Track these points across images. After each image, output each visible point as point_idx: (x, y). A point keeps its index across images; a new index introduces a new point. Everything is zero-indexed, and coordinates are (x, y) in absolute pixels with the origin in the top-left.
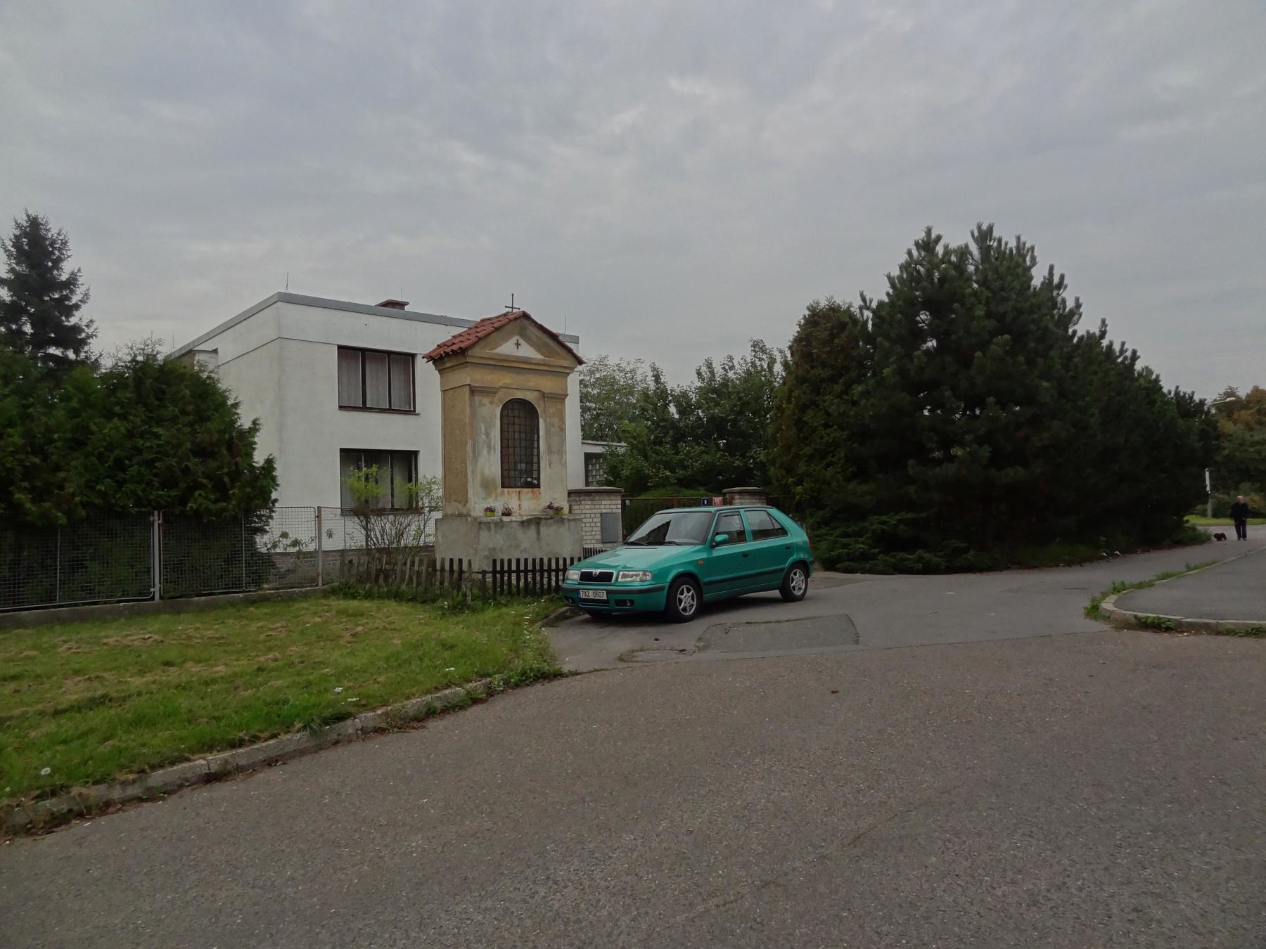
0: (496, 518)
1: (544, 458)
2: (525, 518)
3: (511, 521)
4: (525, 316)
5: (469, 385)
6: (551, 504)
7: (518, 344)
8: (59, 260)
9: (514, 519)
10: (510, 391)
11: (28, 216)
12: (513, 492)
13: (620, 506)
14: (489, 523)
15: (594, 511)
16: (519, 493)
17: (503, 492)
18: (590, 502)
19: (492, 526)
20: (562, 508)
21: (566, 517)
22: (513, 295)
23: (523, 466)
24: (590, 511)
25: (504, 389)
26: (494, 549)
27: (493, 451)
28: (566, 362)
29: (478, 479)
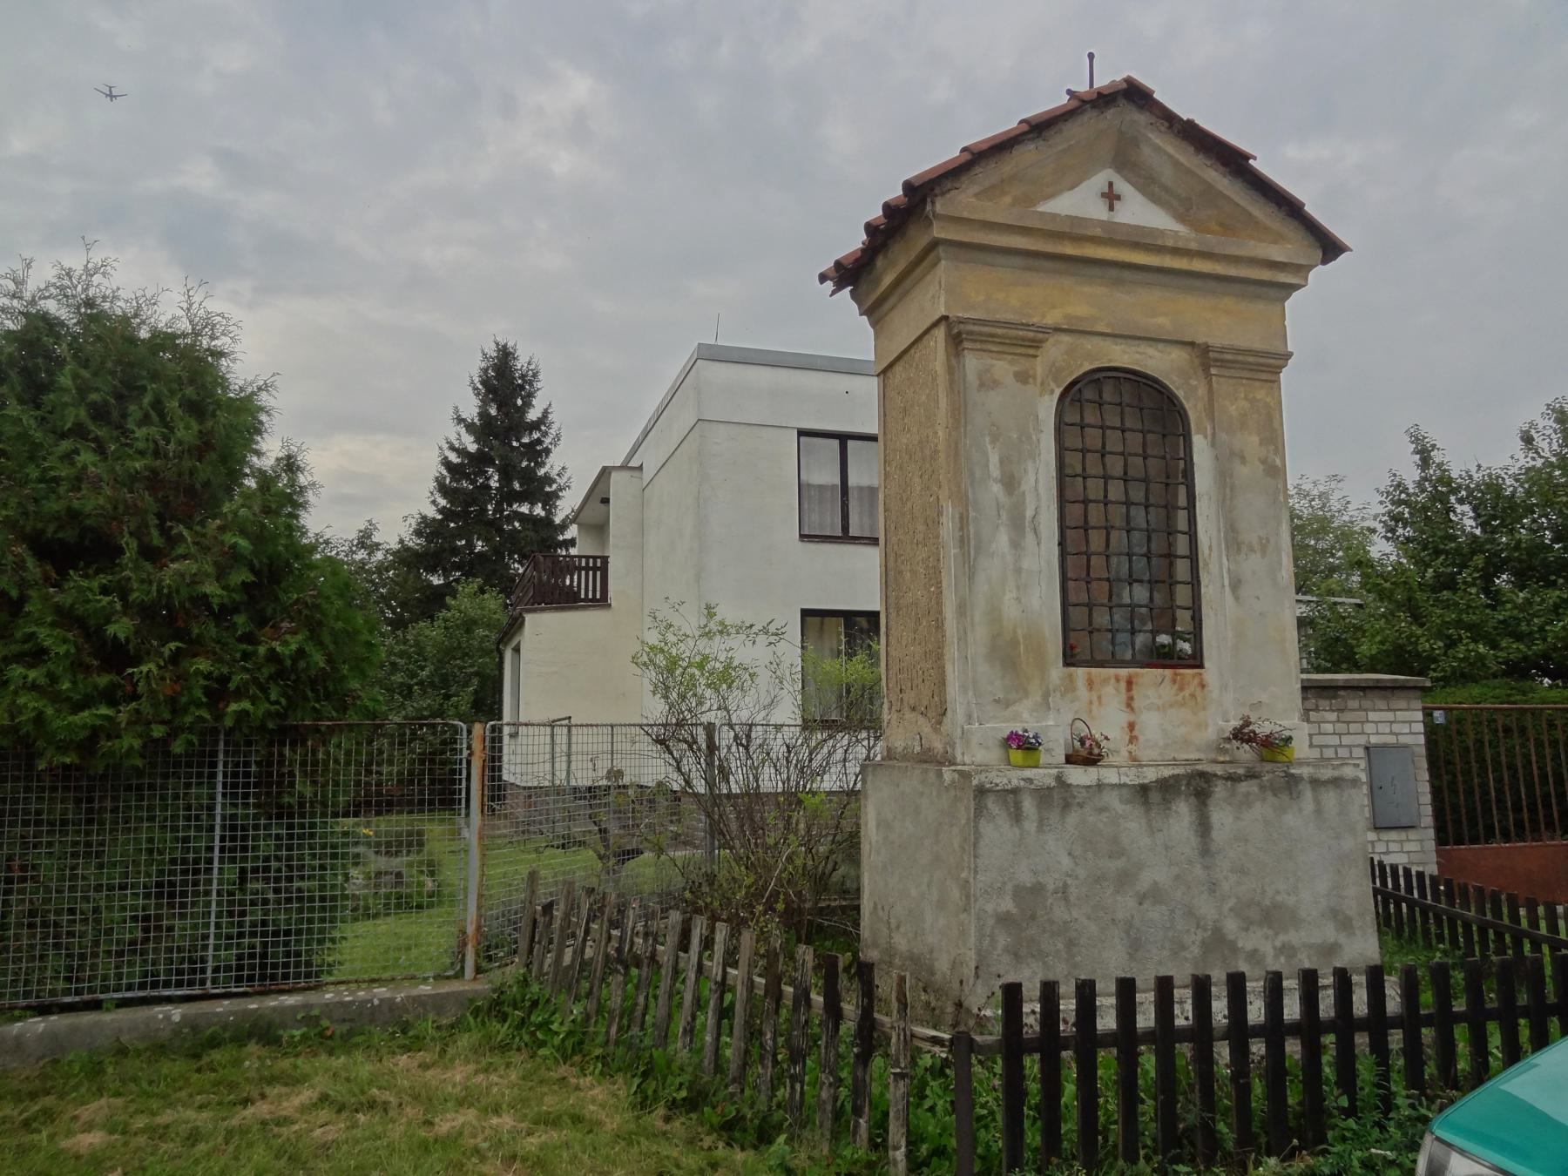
0: (1043, 776)
1: (1214, 568)
2: (1150, 775)
3: (1100, 786)
4: (1134, 94)
5: (945, 318)
6: (1247, 723)
7: (1111, 197)
8: (530, 395)
9: (1111, 776)
10: (1090, 344)
11: (497, 344)
12: (1106, 681)
13: (1420, 728)
14: (1015, 791)
15: (1346, 740)
16: (1130, 683)
17: (1071, 680)
18: (1333, 716)
19: (1028, 805)
20: (1289, 739)
21: (1305, 771)
22: (1091, 56)
23: (1141, 593)
24: (1335, 740)
25: (1066, 338)
26: (1038, 889)
27: (1030, 537)
28: (1289, 247)
29: (980, 635)
